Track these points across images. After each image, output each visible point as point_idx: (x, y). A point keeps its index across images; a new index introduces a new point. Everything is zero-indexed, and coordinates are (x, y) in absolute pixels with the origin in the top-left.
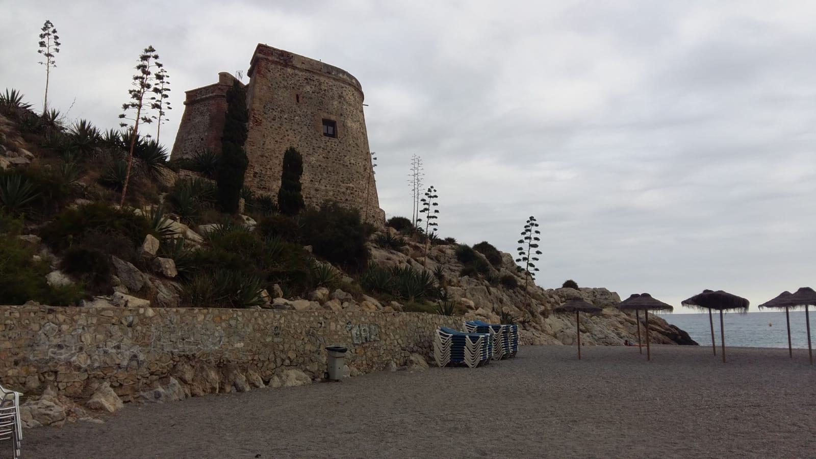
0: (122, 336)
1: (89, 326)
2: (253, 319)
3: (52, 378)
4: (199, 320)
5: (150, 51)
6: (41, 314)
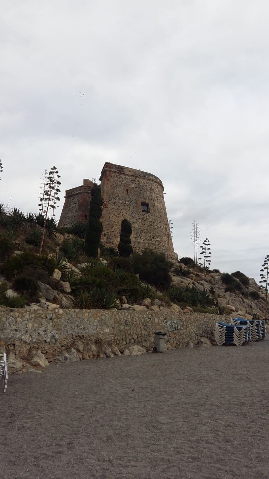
0: (47, 325)
1: (31, 319)
2: (114, 316)
3: (12, 348)
4: (86, 316)
5: (54, 169)
6: (7, 312)
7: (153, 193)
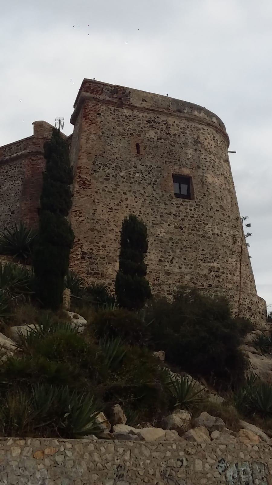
2: (87, 454)
7: (203, 151)
